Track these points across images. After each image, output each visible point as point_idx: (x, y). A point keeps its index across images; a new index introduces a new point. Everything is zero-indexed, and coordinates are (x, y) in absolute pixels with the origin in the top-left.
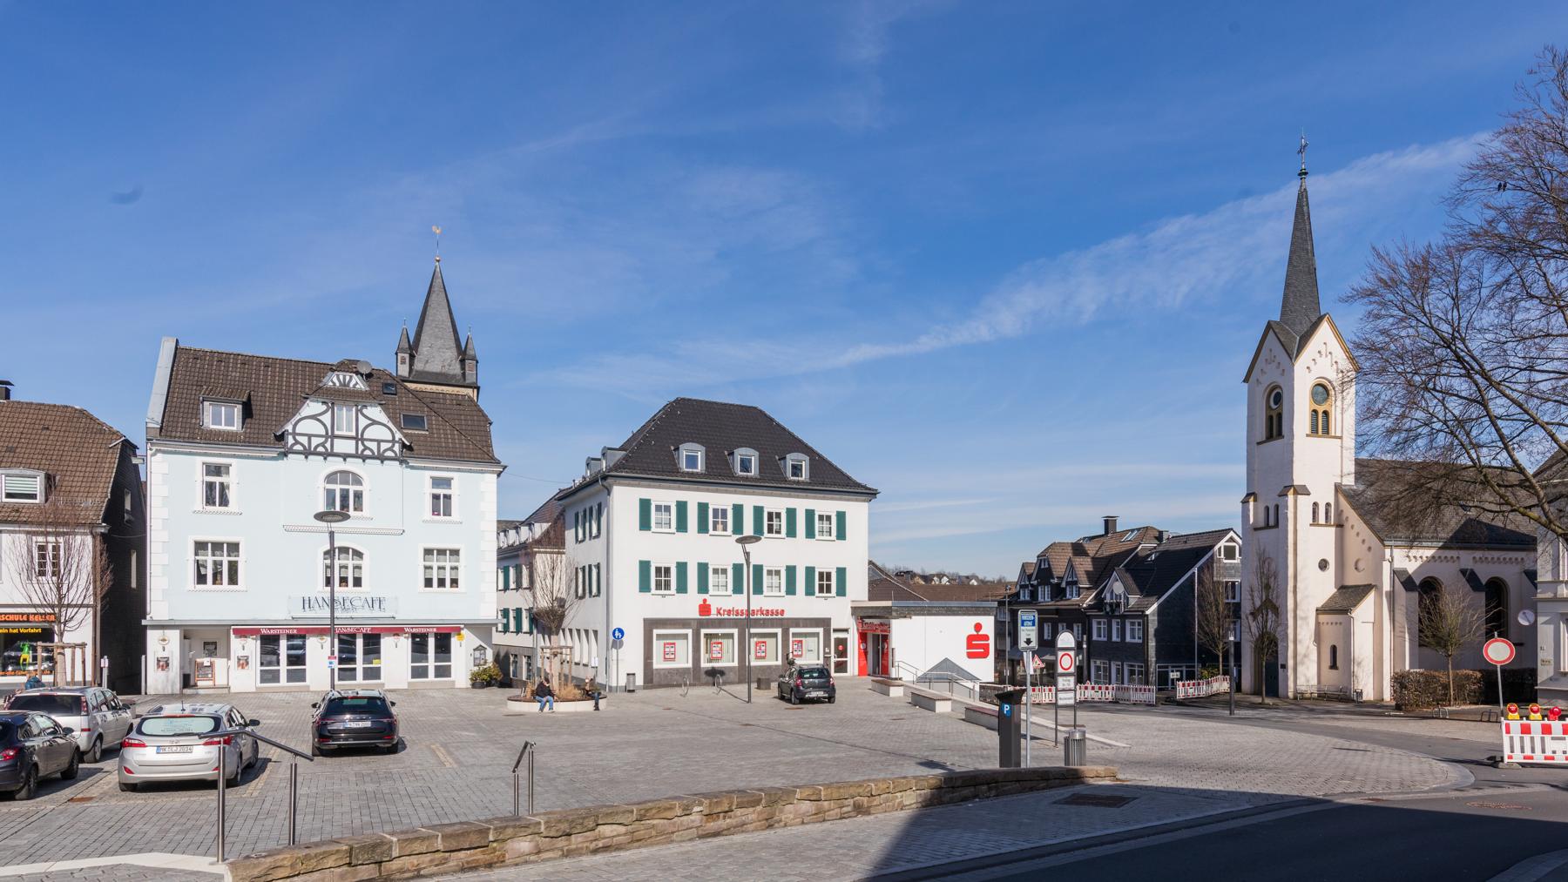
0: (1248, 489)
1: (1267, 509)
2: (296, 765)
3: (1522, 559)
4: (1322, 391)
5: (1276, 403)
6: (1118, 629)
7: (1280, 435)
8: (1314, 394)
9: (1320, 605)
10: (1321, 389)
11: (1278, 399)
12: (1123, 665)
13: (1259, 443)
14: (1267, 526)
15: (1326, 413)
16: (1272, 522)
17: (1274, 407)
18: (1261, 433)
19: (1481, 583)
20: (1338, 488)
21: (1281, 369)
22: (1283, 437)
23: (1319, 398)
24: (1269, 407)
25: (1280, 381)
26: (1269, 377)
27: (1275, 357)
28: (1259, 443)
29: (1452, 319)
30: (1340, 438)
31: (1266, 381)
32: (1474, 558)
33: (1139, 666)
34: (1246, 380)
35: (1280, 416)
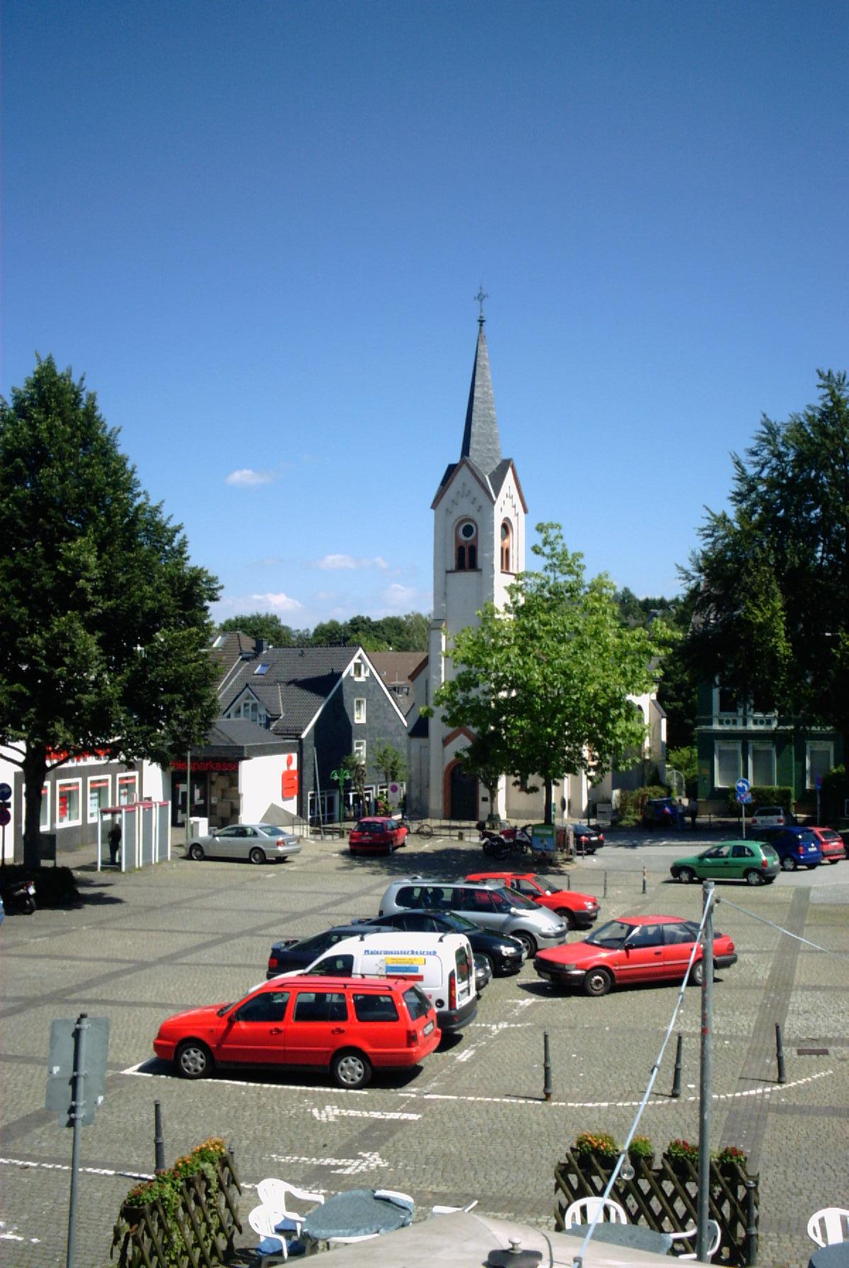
4: (506, 527)
11: (468, 531)
18: (452, 564)
24: (457, 538)
25: (477, 517)
26: (465, 509)
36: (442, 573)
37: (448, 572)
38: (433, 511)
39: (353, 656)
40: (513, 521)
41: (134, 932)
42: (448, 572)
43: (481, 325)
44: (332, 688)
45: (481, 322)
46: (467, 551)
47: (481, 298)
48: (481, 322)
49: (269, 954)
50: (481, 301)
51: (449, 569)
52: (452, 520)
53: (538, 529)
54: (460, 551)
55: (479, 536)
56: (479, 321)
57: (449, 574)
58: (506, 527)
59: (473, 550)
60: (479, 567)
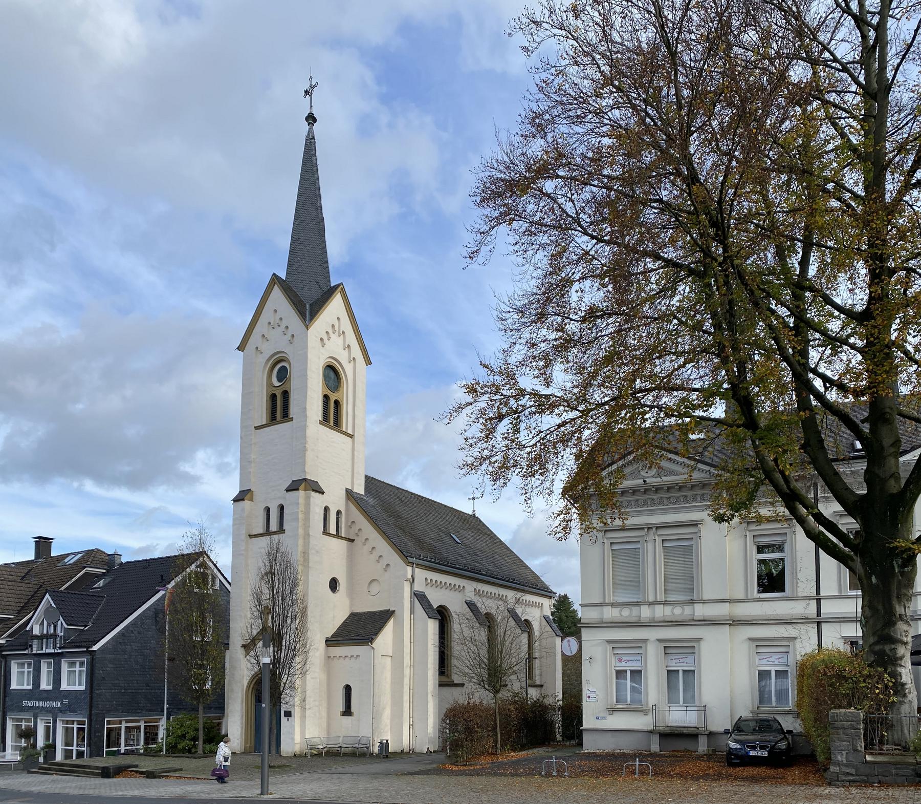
0: (242, 483)
1: (268, 510)
2: (282, 508)
3: (464, 587)
4: (333, 374)
5: (279, 380)
6: (49, 672)
7: (286, 416)
8: (326, 377)
9: (329, 635)
10: (332, 374)
11: (283, 374)
12: (55, 722)
13: (257, 428)
14: (268, 532)
15: (337, 403)
16: (274, 526)
17: (277, 384)
18: (262, 416)
19: (433, 608)
20: (350, 494)
21: (289, 335)
22: (292, 419)
23: (331, 384)
24: (270, 384)
27: (281, 319)
28: (257, 428)
29: (720, 202)
30: (351, 436)
31: (268, 350)
32: (426, 579)
33: (79, 723)
34: (241, 348)
35: (286, 394)
36: (244, 536)
37: (251, 536)
48: (311, 119)
49: (344, 492)
52: (261, 360)
58: (333, 374)
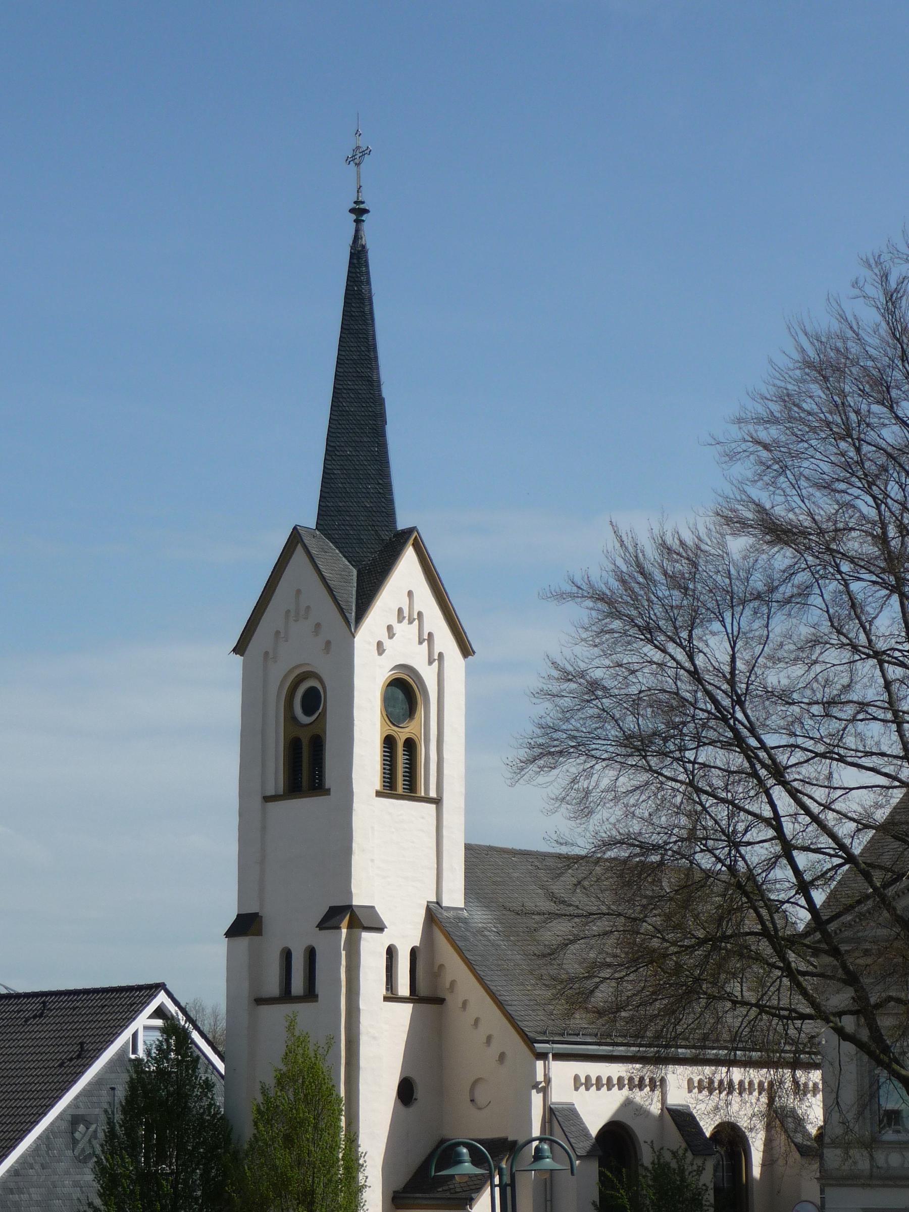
18: (276, 781)
25: (321, 665)
37: (267, 799)
38: (239, 659)
39: (138, 1012)
40: (429, 675)
41: (867, 722)
42: (267, 799)
43: (358, 222)
44: (51, 1106)
45: (359, 212)
46: (385, 762)
47: (357, 157)
50: (358, 165)
51: (271, 792)
52: (279, 672)
53: (388, 626)
54: (293, 748)
55: (326, 711)
56: (352, 211)
57: (271, 805)
59: (318, 744)
60: (327, 787)
